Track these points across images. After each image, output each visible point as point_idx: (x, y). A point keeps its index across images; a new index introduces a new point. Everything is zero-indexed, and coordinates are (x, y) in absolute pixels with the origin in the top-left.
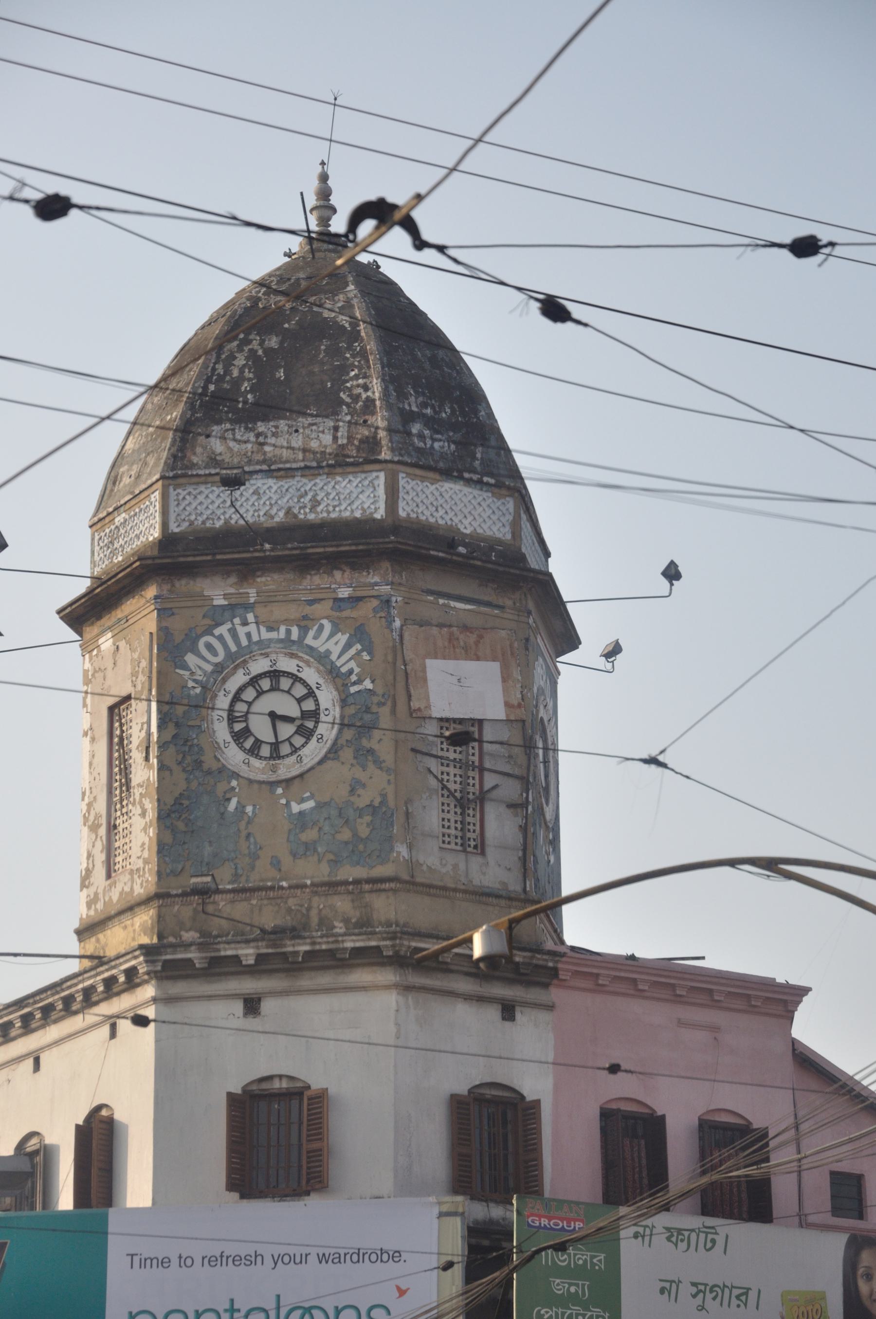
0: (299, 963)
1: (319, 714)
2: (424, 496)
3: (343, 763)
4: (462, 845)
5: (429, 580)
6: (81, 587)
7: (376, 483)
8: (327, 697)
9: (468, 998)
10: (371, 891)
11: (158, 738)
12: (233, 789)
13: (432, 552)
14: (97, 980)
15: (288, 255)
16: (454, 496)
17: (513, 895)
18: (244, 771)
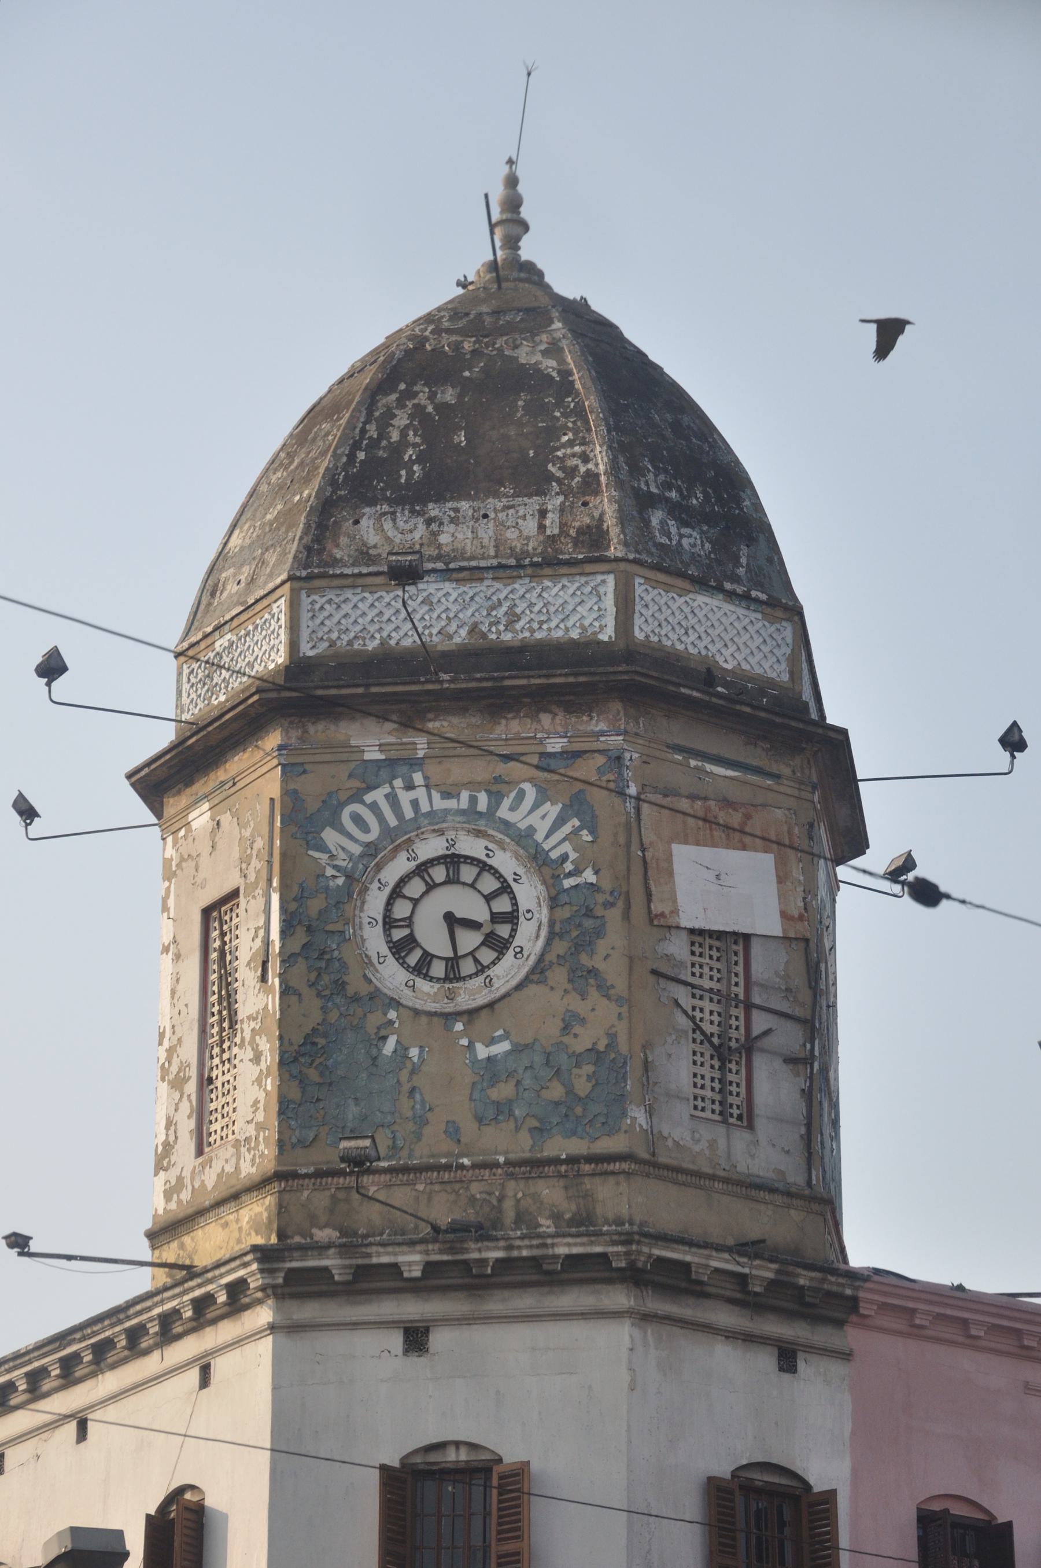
0: (488, 1276)
1: (517, 918)
2: (669, 611)
3: (552, 988)
4: (721, 1113)
5: (676, 731)
6: (161, 737)
7: (602, 590)
8: (529, 893)
9: (730, 1335)
10: (593, 1175)
11: (281, 948)
12: (391, 1022)
13: (683, 690)
14: (182, 1302)
15: (463, 284)
16: (710, 615)
17: (793, 1190)
18: (407, 997)
